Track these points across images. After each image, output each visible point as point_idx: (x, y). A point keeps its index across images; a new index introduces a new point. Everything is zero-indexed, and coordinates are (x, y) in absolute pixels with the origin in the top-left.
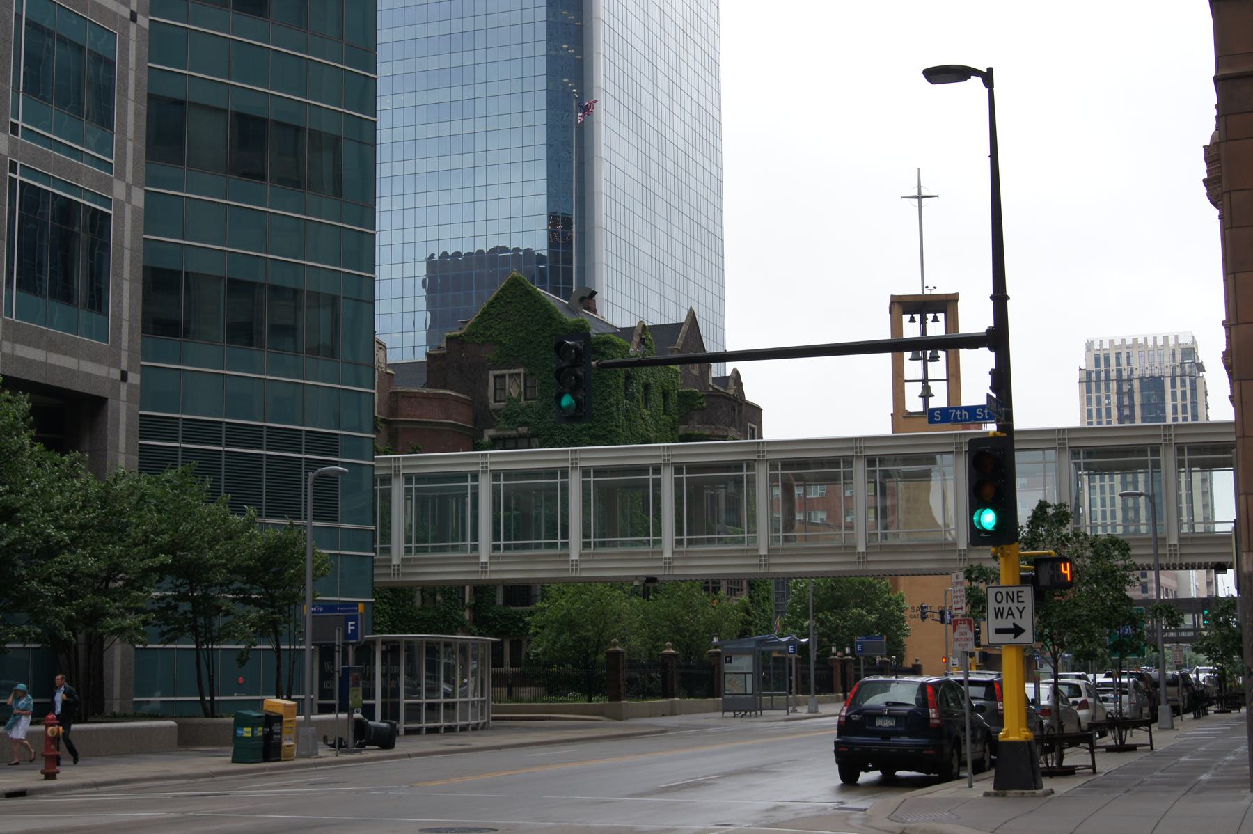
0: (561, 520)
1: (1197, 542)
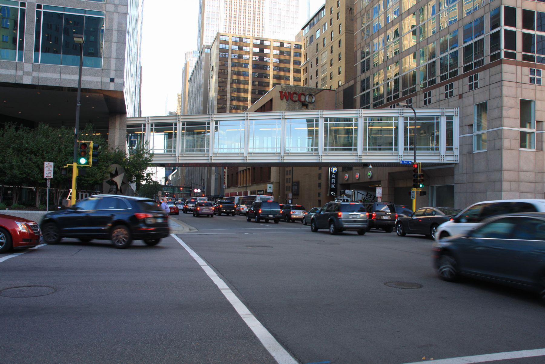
0: (536, 139)
1: (290, 155)
